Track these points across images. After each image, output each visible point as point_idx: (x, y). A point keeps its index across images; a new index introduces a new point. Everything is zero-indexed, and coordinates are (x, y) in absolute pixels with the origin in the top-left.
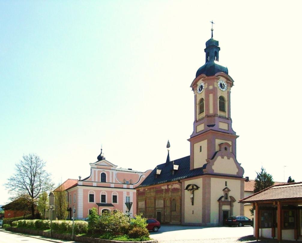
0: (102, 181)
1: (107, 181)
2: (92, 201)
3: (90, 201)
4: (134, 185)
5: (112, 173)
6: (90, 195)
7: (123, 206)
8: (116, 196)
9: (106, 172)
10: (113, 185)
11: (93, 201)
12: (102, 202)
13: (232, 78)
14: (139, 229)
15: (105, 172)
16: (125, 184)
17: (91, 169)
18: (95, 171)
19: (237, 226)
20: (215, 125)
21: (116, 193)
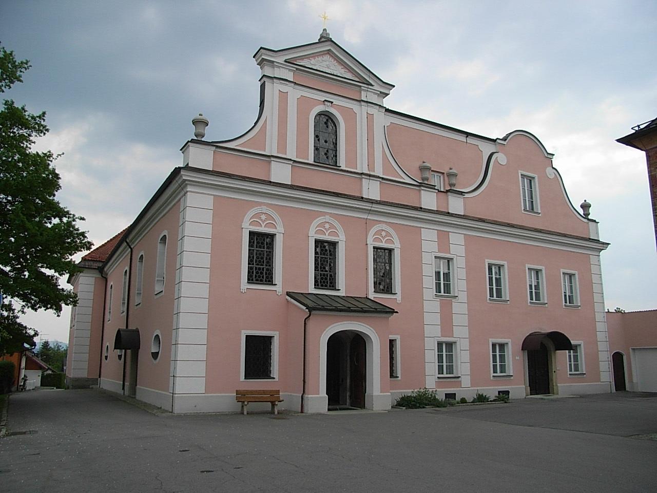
0: (318, 162)
1: (342, 164)
2: (447, 395)
3: (250, 280)
4: (466, 196)
5: (370, 117)
6: (252, 234)
7: (421, 312)
8: (334, 244)
9: (339, 107)
10: (372, 190)
11: (269, 280)
12: (317, 285)
13: (263, 114)
14: (40, 122)
15: (332, 110)
16: (423, 185)
17: (263, 87)
18: (283, 96)
19: (318, 250)
20: (388, 94)
21: (269, 217)
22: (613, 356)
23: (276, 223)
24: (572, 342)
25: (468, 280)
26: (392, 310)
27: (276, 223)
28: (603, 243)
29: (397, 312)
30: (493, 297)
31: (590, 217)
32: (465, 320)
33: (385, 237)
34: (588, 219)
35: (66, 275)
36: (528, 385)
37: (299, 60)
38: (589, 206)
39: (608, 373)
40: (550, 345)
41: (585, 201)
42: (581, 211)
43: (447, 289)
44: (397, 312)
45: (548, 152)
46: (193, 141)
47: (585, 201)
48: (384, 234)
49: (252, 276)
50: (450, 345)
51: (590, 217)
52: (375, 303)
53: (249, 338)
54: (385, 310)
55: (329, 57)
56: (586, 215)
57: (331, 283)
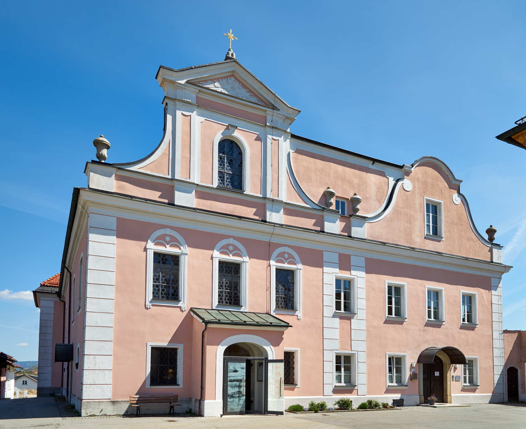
22: (508, 370)
23: (242, 253)
24: (466, 356)
25: (368, 299)
26: (286, 324)
27: (242, 253)
28: (506, 267)
29: (291, 326)
30: (391, 314)
31: (494, 242)
32: (363, 336)
33: (232, 251)
34: (493, 244)
35: (175, 183)
36: (422, 394)
37: (201, 81)
38: (495, 231)
39: (502, 385)
40: (445, 358)
41: (491, 226)
42: (486, 237)
43: (347, 307)
44: (291, 326)
45: (456, 178)
46: (93, 162)
47: (491, 226)
48: (286, 256)
49: (157, 294)
50: (348, 359)
51: (494, 242)
52: (420, 380)
53: (153, 349)
54: (280, 324)
55: (233, 79)
56: (491, 239)
57: (235, 300)
